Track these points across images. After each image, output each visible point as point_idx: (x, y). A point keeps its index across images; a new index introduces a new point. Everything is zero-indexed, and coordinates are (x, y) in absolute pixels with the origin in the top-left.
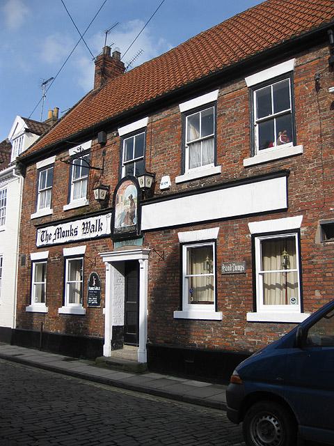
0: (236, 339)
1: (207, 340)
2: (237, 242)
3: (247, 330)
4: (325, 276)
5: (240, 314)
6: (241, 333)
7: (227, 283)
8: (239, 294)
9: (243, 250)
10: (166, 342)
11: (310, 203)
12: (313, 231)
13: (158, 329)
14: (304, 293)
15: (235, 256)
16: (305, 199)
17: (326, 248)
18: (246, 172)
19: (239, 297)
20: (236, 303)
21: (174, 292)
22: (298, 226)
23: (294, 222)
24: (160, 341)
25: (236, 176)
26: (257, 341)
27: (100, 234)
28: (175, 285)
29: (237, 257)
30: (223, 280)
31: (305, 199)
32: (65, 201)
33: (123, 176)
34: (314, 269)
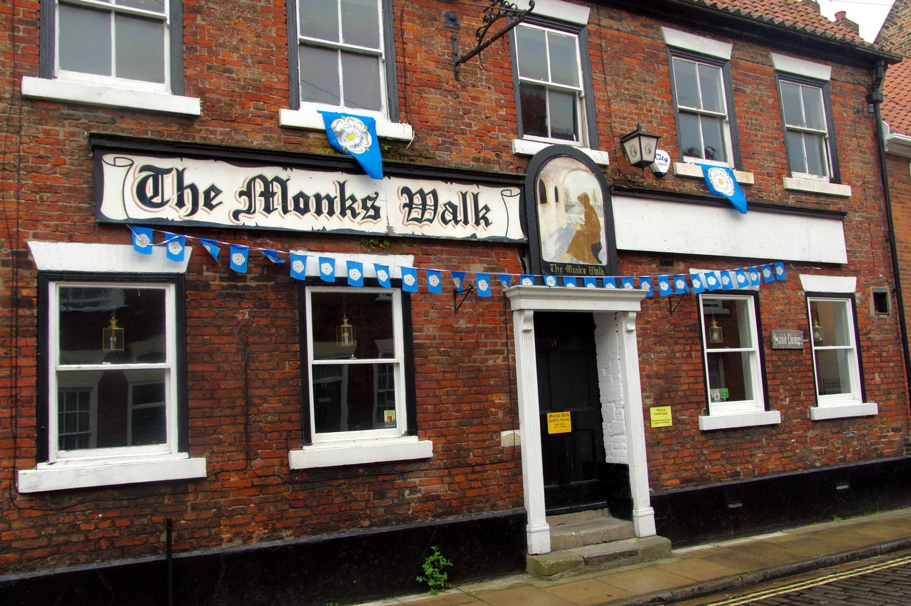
0: (797, 451)
1: (757, 460)
2: (788, 301)
3: (811, 434)
4: (881, 356)
5: (800, 412)
6: (802, 440)
7: (780, 363)
8: (797, 381)
9: (796, 314)
10: (685, 481)
11: (861, 263)
12: (867, 300)
13: (665, 457)
14: (866, 376)
15: (786, 321)
16: (856, 257)
17: (880, 322)
18: (787, 198)
19: (796, 384)
20: (794, 394)
21: (692, 380)
22: (852, 289)
23: (847, 284)
24: (672, 485)
25: (775, 199)
26: (823, 448)
27: (482, 233)
28: (692, 367)
29: (790, 324)
30: (775, 358)
31: (856, 257)
32: (29, 444)
33: (207, 95)
34: (872, 347)
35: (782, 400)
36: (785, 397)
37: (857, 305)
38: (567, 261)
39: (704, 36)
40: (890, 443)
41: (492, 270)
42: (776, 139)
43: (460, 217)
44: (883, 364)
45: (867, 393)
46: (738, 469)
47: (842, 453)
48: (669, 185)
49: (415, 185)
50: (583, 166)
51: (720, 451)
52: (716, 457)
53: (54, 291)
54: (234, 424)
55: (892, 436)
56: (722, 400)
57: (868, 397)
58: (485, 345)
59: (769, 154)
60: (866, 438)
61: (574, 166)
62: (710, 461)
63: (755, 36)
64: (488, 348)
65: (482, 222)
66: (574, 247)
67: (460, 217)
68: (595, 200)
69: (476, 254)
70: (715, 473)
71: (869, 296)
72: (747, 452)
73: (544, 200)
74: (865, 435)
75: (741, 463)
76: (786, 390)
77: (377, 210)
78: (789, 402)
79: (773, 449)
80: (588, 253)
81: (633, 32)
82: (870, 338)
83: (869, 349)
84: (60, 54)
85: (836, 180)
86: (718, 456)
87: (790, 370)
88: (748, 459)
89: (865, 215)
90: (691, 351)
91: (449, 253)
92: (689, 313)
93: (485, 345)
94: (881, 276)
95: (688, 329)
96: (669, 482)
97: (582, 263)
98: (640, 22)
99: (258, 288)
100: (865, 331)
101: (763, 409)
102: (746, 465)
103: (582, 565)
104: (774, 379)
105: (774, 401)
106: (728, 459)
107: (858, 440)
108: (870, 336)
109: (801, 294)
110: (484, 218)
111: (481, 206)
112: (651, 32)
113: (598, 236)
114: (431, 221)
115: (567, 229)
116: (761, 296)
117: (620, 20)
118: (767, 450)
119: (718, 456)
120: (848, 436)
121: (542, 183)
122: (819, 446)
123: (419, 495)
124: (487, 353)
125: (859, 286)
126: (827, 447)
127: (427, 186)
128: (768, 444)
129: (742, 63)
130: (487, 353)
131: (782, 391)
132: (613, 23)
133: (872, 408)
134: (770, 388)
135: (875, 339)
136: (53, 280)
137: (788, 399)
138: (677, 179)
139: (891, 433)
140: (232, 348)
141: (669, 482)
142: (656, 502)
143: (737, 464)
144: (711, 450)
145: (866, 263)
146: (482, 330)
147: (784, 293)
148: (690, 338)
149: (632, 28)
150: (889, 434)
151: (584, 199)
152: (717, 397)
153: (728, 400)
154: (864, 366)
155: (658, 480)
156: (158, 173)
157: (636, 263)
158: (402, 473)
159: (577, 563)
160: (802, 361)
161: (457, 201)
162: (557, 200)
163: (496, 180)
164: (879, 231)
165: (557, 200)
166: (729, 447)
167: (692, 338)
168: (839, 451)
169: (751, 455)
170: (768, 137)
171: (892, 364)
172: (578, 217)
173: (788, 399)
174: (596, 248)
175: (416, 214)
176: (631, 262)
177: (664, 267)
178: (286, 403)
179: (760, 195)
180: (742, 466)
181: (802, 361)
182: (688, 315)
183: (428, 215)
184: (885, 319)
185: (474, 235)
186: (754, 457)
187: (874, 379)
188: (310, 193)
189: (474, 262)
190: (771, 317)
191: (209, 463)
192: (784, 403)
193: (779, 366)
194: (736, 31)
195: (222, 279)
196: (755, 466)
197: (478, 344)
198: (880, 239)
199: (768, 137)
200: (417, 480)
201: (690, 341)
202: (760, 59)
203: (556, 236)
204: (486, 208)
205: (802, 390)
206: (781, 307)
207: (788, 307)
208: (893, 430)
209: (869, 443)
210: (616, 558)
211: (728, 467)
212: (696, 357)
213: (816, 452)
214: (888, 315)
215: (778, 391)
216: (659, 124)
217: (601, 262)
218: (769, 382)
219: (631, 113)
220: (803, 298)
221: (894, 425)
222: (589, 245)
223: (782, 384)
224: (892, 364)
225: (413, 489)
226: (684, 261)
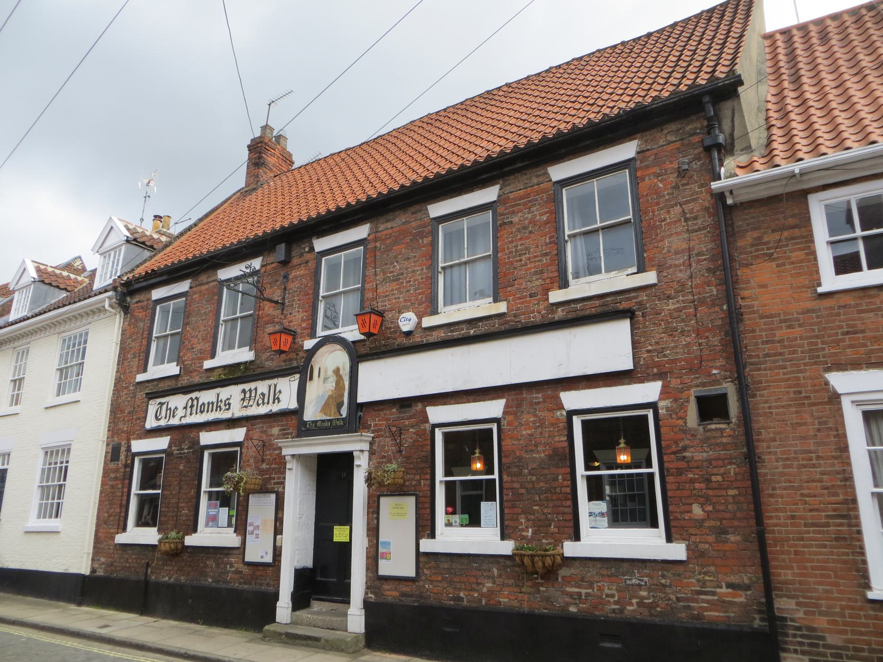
4: (708, 481)
7: (523, 491)
12: (683, 407)
15: (536, 446)
16: (665, 356)
26: (583, 591)
27: (275, 408)
31: (665, 356)
35: (522, 530)
36: (527, 527)
37: (661, 417)
38: (318, 419)
39: (472, 191)
40: (722, 604)
41: (284, 430)
42: (546, 254)
43: (266, 401)
44: (710, 492)
45: (673, 530)
46: (462, 594)
47: (616, 603)
48: (417, 339)
49: (246, 386)
50: (339, 347)
51: (441, 574)
52: (436, 579)
53: (577, 422)
54: (172, 520)
55: (727, 595)
56: (462, 526)
57: (674, 535)
58: (274, 479)
59: (536, 273)
60: (668, 590)
61: (333, 349)
62: (431, 582)
63: (588, 142)
64: (276, 481)
65: (276, 401)
66: (325, 409)
67: (266, 401)
68: (344, 369)
69: (275, 421)
70: (435, 594)
71: (688, 401)
72: (473, 580)
73: (311, 378)
74: (664, 586)
75: (465, 589)
76: (528, 520)
77: (229, 404)
78: (533, 533)
79: (506, 581)
80: (334, 409)
81: (404, 224)
82: (684, 457)
83: (680, 472)
84: (239, 341)
85: (641, 270)
86: (439, 578)
87: (537, 498)
88: (474, 586)
89: (690, 297)
90: (421, 480)
91: (263, 423)
92: (422, 446)
93: (274, 479)
94: (715, 371)
95: (418, 460)
96: (389, 593)
97: (328, 418)
98: (410, 212)
99: (188, 453)
100: (674, 448)
101: (499, 538)
102: (471, 593)
103: (283, 637)
104: (513, 507)
105: (511, 531)
106: (451, 582)
107: (650, 590)
108: (686, 454)
109: (428, 427)
110: (278, 398)
111: (277, 391)
112: (419, 215)
113: (343, 395)
114: (251, 406)
115: (322, 395)
116: (504, 422)
117: (394, 219)
118: (499, 581)
119: (439, 578)
120: (628, 582)
121: (312, 366)
122: (576, 587)
123: (233, 569)
124: (275, 484)
125: (665, 393)
126: (590, 591)
127: (252, 385)
128: (500, 576)
129: (512, 196)
130: (275, 484)
131: (523, 521)
132: (389, 225)
133: (678, 551)
134: (506, 517)
135: (696, 458)
136: (437, 427)
137: (530, 530)
138: (426, 331)
139: (724, 590)
140: (176, 483)
141: (389, 593)
142: (367, 605)
143: (460, 590)
144: (433, 571)
145: (684, 360)
146: (274, 469)
147: (536, 416)
148: (419, 468)
149: (404, 220)
150: (718, 590)
151: (337, 371)
152: (456, 522)
153: (466, 526)
154: (669, 494)
155: (379, 589)
156: (161, 404)
157: (378, 410)
158: (228, 555)
159: (280, 634)
160: (555, 488)
161: (266, 392)
162: (319, 377)
163: (191, 389)
164: (715, 315)
165: (319, 377)
166: (452, 571)
167: (423, 468)
168: (612, 600)
169: (478, 584)
170: (536, 257)
171: (731, 492)
172: (331, 385)
173: (530, 530)
174: (340, 405)
175: (245, 404)
176: (375, 410)
177: (403, 410)
178: (190, 511)
179: (517, 320)
180: (466, 593)
181: (555, 488)
182: (420, 449)
183: (251, 403)
184: (722, 430)
185: (271, 410)
186: (481, 586)
187: (690, 512)
188: (206, 402)
189: (274, 427)
190: (516, 442)
191: (688, 548)
192: (524, 534)
193: (522, 494)
194: (494, 173)
195: (178, 450)
196: (482, 595)
197: (270, 478)
198: (719, 322)
199: (536, 257)
200: (233, 560)
201: (419, 471)
202: (535, 180)
203: (314, 403)
204: (280, 392)
205: (554, 521)
206: (529, 432)
207: (540, 430)
208: (729, 586)
209: (673, 597)
210: (305, 639)
211: (451, 590)
212: (424, 485)
213: (571, 595)
214: (728, 424)
215: (517, 520)
216: (415, 290)
217: (342, 415)
218: (506, 511)
219: (393, 290)
220: (564, 418)
221: (733, 579)
222: (335, 404)
223: (523, 512)
224: (731, 492)
225: (232, 565)
226: (422, 402)
